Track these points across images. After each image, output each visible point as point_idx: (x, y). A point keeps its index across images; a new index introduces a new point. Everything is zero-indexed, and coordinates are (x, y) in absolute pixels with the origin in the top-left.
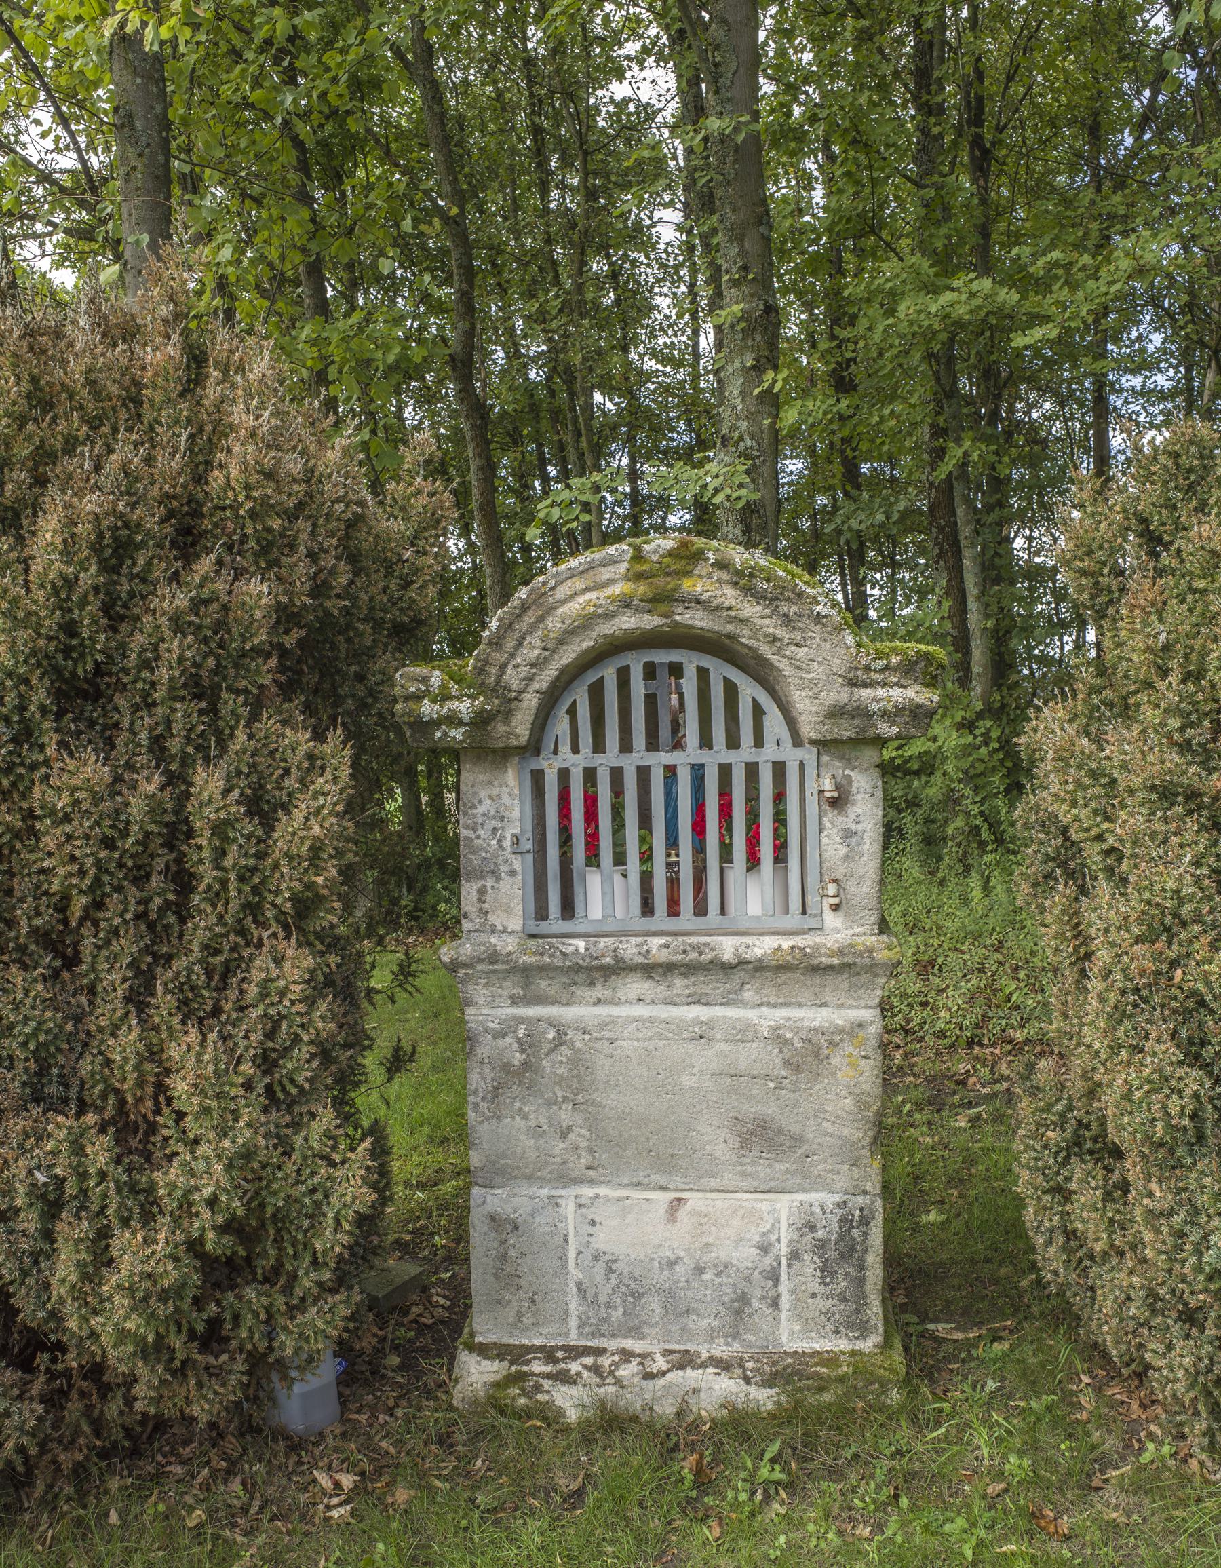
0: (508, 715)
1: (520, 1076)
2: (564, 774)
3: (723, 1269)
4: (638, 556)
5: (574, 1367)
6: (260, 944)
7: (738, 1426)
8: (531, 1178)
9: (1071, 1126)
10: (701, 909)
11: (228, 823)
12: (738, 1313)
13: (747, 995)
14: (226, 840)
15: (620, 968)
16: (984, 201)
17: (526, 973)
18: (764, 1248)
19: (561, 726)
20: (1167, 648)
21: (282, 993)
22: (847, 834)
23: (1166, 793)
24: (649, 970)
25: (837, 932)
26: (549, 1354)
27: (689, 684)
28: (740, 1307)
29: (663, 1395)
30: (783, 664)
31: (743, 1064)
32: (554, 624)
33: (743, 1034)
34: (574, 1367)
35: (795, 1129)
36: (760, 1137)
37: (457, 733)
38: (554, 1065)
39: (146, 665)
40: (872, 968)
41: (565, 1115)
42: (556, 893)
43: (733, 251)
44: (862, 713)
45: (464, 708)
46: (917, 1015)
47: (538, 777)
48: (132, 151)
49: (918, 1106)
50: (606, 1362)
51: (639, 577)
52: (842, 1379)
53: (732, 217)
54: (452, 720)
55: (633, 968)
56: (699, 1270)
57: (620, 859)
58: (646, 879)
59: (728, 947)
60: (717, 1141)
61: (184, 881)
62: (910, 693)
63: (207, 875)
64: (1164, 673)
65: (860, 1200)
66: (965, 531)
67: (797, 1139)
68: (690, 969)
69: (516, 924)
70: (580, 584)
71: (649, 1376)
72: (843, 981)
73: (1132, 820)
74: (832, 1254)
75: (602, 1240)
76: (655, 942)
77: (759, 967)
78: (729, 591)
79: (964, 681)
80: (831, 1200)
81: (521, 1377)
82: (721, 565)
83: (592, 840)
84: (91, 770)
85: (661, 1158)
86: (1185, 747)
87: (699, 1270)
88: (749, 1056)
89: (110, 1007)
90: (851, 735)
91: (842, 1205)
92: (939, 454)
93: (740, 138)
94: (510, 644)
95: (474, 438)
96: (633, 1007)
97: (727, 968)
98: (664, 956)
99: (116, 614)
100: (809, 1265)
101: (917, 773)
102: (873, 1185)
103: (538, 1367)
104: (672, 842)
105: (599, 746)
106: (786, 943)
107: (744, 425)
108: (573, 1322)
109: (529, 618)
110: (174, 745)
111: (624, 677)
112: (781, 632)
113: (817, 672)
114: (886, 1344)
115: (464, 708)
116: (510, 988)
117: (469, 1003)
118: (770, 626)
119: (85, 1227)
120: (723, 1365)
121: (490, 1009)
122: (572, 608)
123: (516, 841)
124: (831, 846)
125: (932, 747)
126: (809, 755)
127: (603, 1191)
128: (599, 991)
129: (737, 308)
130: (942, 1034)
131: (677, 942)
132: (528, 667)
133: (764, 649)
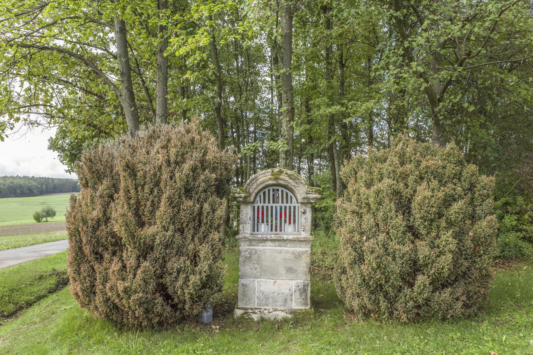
0: (250, 196)
1: (248, 259)
2: (258, 207)
3: (283, 294)
4: (273, 172)
5: (256, 311)
6: (211, 232)
7: (285, 321)
8: (250, 277)
9: (342, 269)
10: (281, 230)
11: (209, 212)
12: (285, 302)
13: (288, 245)
14: (208, 215)
15: (267, 240)
16: (342, 76)
17: (251, 240)
18: (290, 290)
19: (258, 199)
20: (355, 190)
21: (215, 240)
22: (306, 218)
23: (353, 212)
24: (272, 240)
25: (304, 235)
26: (252, 309)
27: (280, 193)
28: (285, 301)
29: (271, 316)
30: (296, 190)
31: (287, 257)
32: (258, 182)
33: (287, 252)
34: (256, 311)
35: (296, 269)
36: (290, 270)
37: (241, 199)
38: (255, 257)
39: (197, 187)
40: (309, 241)
41: (256, 266)
42: (255, 228)
43: (285, 96)
44: (308, 198)
45: (243, 195)
46: (321, 263)
47: (254, 207)
48: (160, 73)
49: (320, 280)
50: (262, 310)
51: (273, 175)
52: (303, 313)
53: (285, 89)
54: (241, 197)
55: (269, 240)
56: (279, 294)
57: (267, 222)
58: (272, 225)
59: (285, 237)
60: (283, 271)
61: (200, 222)
62: (316, 195)
63: (205, 220)
64: (354, 194)
65: (307, 282)
66: (335, 156)
67: (296, 271)
68: (279, 240)
69: (249, 232)
70: (263, 176)
71: (270, 312)
72: (304, 243)
73: (349, 216)
74: (302, 291)
75: (262, 288)
76: (273, 236)
77: (290, 240)
78: (287, 178)
79: (335, 190)
80: (302, 281)
81: (247, 313)
82: (286, 174)
83: (263, 218)
84: (191, 203)
85: (272, 274)
86: (357, 205)
87: (279, 294)
88: (288, 256)
89: (188, 241)
90: (306, 202)
91: (304, 282)
92: (330, 138)
93: (287, 74)
94: (251, 185)
95: (220, 126)
96: (269, 247)
97: (285, 240)
98: (274, 238)
99: (194, 179)
100: (298, 293)
101: (323, 211)
102: (309, 279)
103: (250, 311)
104: (276, 219)
105: (264, 202)
106: (295, 236)
107: (286, 133)
108: (256, 303)
109: (254, 181)
110: (200, 200)
111: (269, 190)
112: (295, 185)
113: (301, 191)
114: (311, 308)
115: (243, 195)
116: (248, 243)
117: (240, 246)
118: (294, 184)
119: (185, 275)
120: (283, 311)
121: (244, 247)
122: (261, 180)
123: (250, 218)
124: (303, 220)
125: (327, 205)
126: (300, 205)
127: (262, 279)
128: (263, 244)
129: (285, 108)
130: (326, 267)
131: (277, 236)
132: (254, 189)
133: (293, 187)
